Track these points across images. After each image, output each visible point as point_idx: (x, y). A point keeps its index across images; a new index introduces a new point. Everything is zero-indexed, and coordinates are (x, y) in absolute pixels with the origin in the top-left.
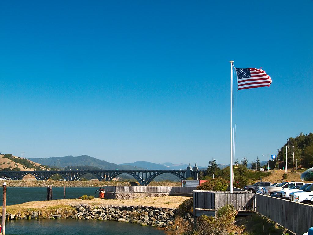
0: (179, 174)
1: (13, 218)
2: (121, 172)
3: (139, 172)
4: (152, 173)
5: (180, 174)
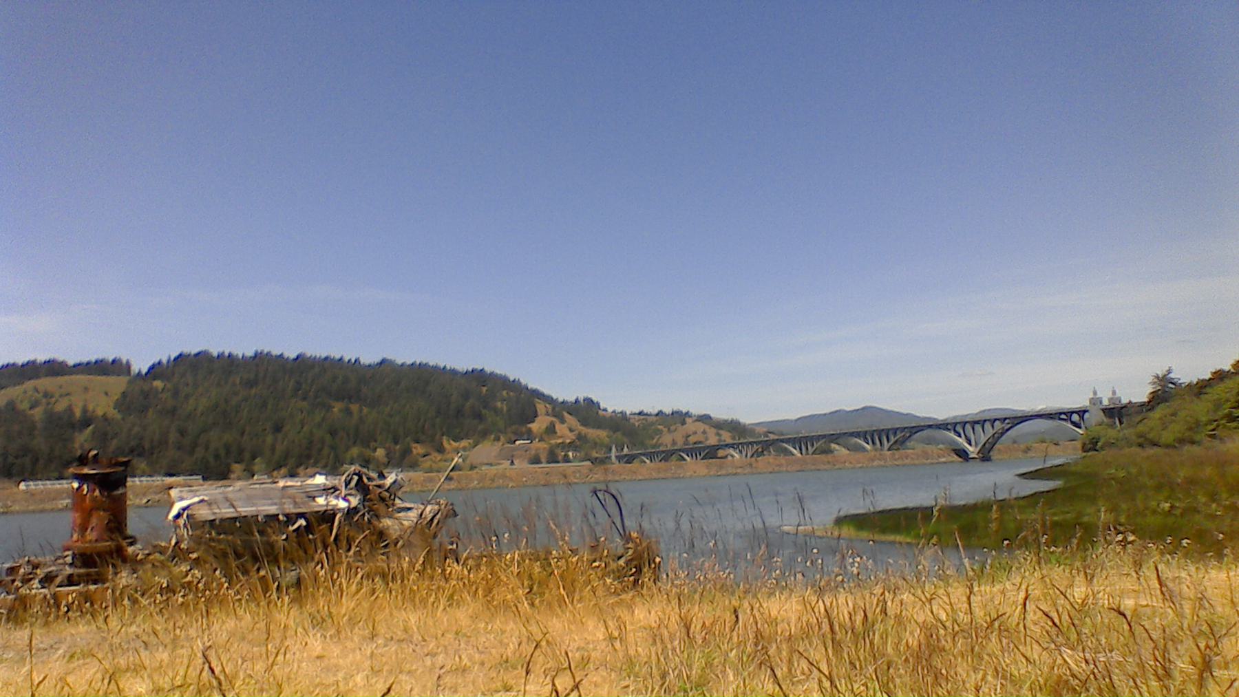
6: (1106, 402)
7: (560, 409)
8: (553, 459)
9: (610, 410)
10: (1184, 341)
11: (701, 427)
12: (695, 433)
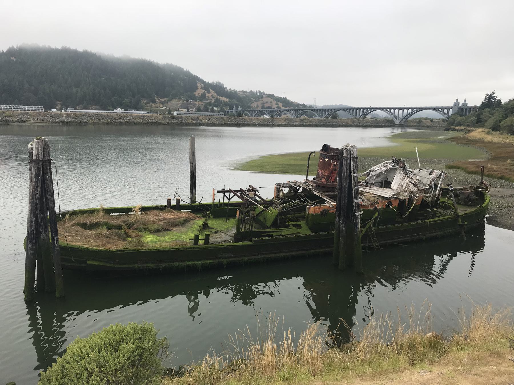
0: (442, 111)
2: (375, 109)
3: (395, 109)
5: (444, 111)
6: (460, 105)
7: (207, 86)
8: (206, 110)
9: (228, 89)
10: (501, 178)
11: (270, 100)
12: (267, 102)
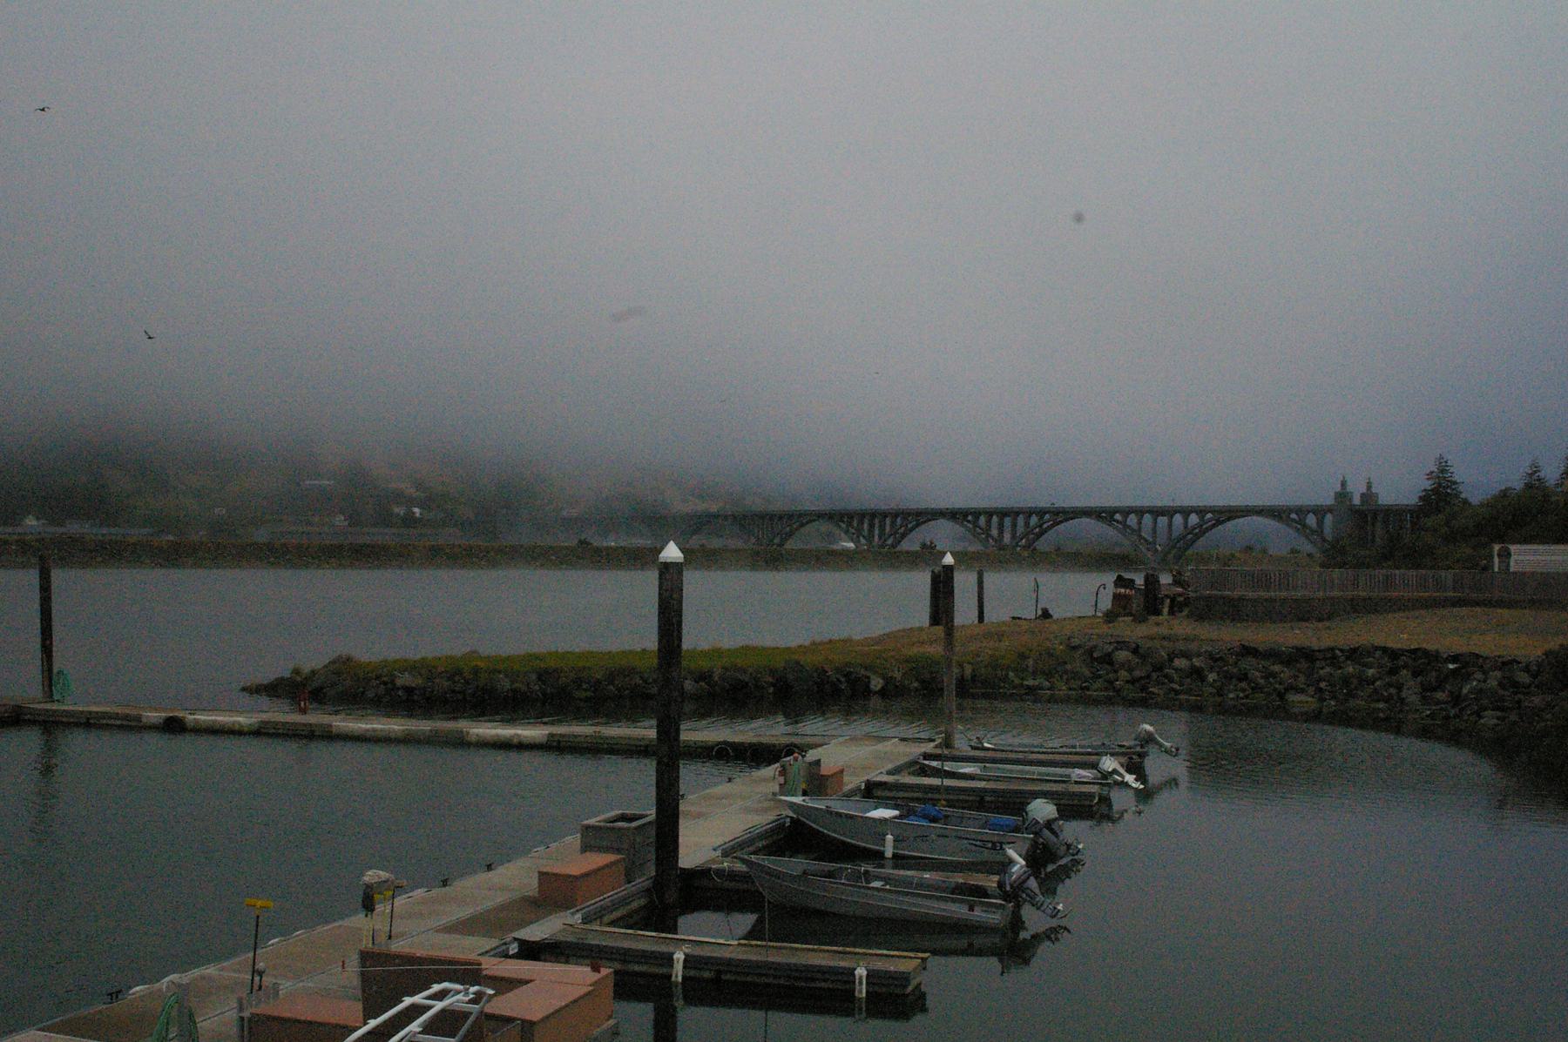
1: (877, 689)
4: (1194, 519)
